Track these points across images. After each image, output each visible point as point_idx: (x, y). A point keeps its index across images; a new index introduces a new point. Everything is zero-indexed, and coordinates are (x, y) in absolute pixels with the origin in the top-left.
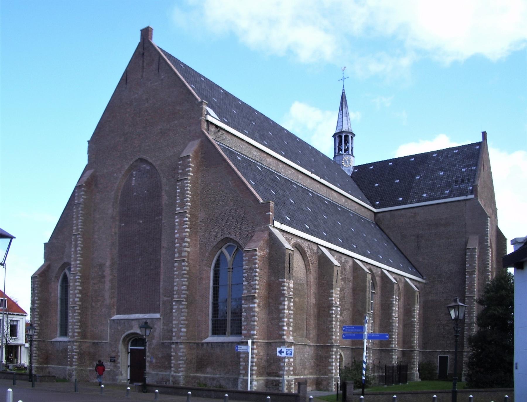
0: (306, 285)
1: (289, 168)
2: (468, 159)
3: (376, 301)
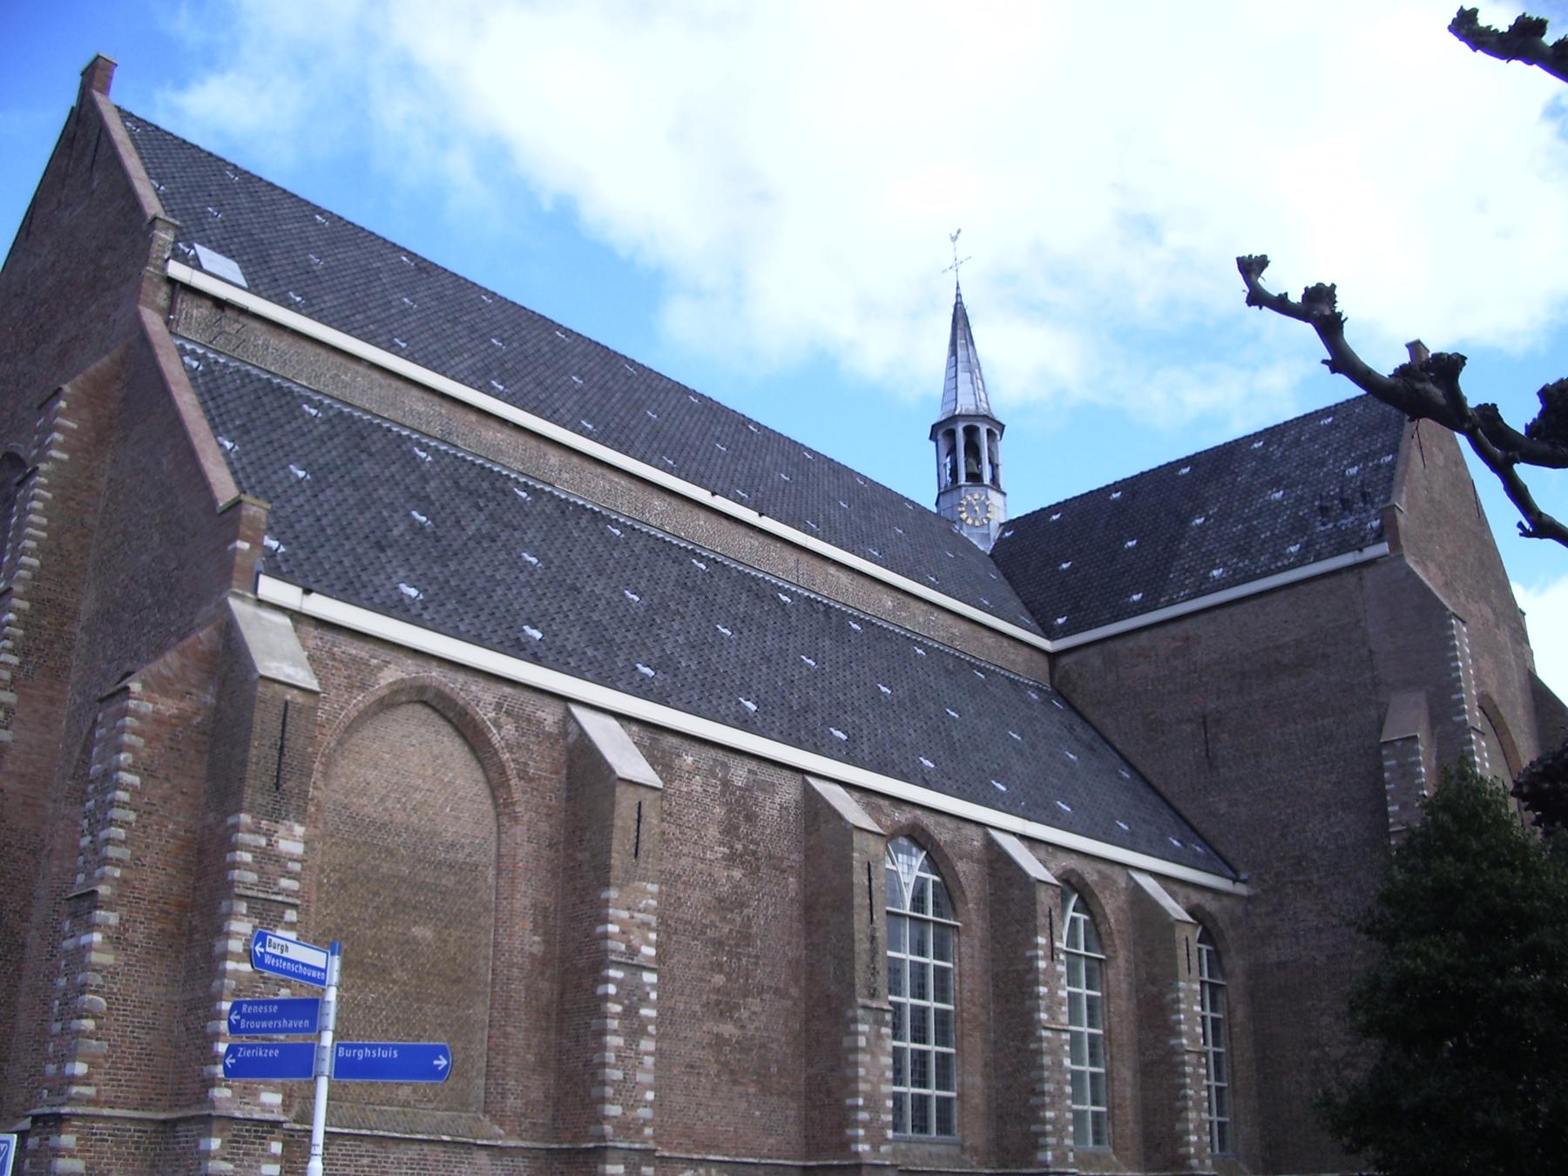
0: (491, 873)
1: (599, 470)
2: (1365, 436)
3: (967, 965)
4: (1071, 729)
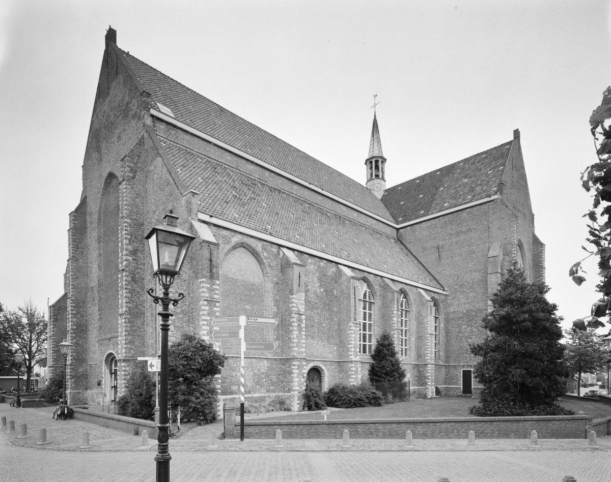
4: (402, 250)
